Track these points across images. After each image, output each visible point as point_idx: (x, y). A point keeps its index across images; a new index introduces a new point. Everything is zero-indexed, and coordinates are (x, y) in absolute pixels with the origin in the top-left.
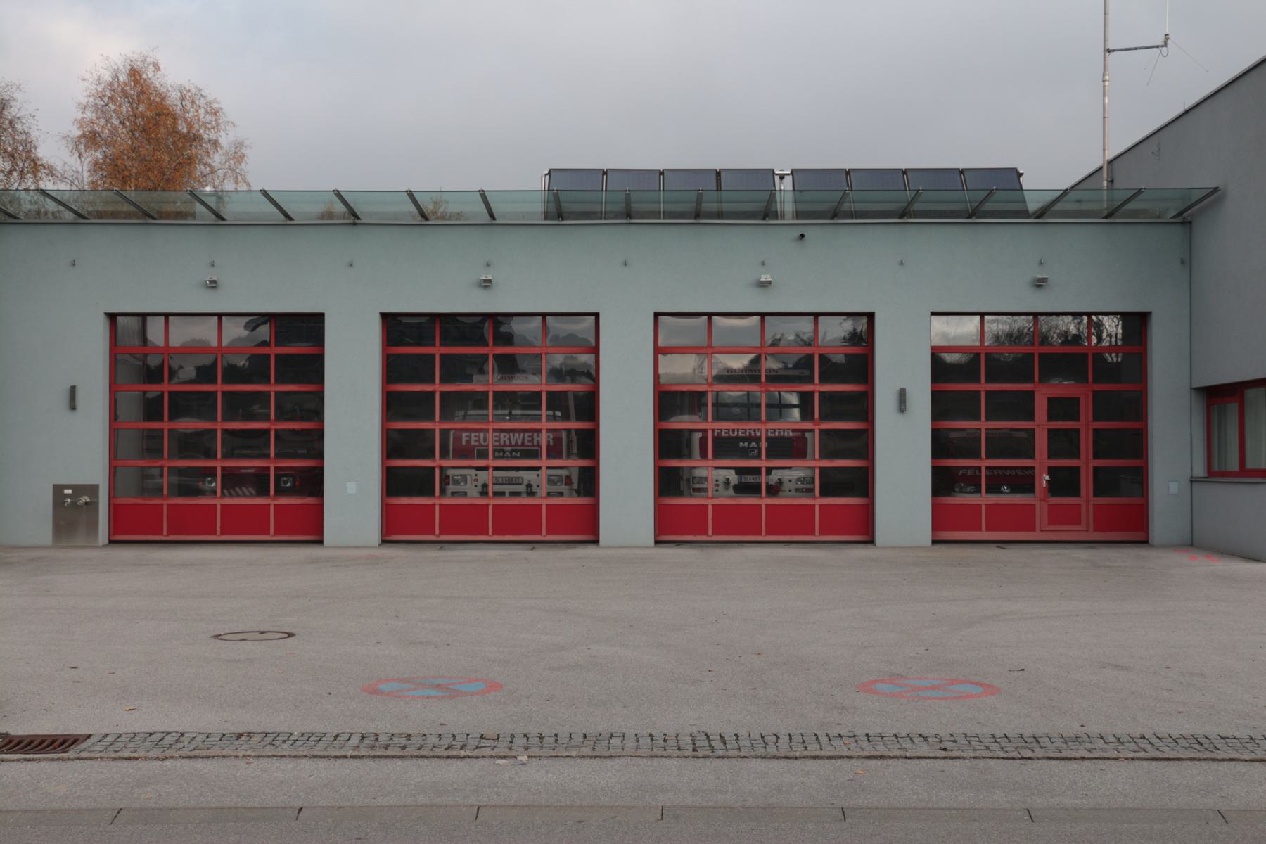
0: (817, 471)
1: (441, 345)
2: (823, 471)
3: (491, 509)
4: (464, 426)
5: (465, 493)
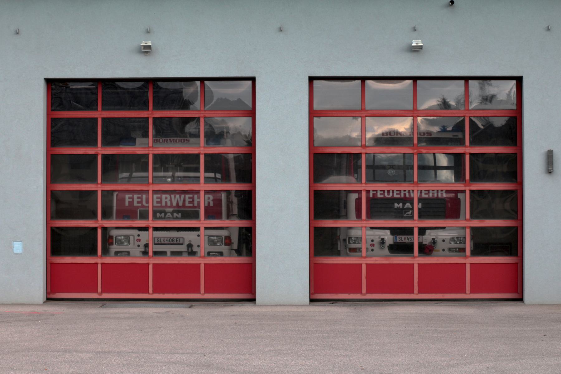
0: (468, 231)
1: (103, 109)
2: (474, 230)
3: (151, 267)
4: (123, 186)
5: (129, 253)
